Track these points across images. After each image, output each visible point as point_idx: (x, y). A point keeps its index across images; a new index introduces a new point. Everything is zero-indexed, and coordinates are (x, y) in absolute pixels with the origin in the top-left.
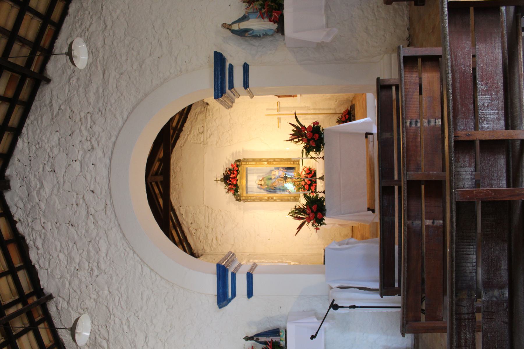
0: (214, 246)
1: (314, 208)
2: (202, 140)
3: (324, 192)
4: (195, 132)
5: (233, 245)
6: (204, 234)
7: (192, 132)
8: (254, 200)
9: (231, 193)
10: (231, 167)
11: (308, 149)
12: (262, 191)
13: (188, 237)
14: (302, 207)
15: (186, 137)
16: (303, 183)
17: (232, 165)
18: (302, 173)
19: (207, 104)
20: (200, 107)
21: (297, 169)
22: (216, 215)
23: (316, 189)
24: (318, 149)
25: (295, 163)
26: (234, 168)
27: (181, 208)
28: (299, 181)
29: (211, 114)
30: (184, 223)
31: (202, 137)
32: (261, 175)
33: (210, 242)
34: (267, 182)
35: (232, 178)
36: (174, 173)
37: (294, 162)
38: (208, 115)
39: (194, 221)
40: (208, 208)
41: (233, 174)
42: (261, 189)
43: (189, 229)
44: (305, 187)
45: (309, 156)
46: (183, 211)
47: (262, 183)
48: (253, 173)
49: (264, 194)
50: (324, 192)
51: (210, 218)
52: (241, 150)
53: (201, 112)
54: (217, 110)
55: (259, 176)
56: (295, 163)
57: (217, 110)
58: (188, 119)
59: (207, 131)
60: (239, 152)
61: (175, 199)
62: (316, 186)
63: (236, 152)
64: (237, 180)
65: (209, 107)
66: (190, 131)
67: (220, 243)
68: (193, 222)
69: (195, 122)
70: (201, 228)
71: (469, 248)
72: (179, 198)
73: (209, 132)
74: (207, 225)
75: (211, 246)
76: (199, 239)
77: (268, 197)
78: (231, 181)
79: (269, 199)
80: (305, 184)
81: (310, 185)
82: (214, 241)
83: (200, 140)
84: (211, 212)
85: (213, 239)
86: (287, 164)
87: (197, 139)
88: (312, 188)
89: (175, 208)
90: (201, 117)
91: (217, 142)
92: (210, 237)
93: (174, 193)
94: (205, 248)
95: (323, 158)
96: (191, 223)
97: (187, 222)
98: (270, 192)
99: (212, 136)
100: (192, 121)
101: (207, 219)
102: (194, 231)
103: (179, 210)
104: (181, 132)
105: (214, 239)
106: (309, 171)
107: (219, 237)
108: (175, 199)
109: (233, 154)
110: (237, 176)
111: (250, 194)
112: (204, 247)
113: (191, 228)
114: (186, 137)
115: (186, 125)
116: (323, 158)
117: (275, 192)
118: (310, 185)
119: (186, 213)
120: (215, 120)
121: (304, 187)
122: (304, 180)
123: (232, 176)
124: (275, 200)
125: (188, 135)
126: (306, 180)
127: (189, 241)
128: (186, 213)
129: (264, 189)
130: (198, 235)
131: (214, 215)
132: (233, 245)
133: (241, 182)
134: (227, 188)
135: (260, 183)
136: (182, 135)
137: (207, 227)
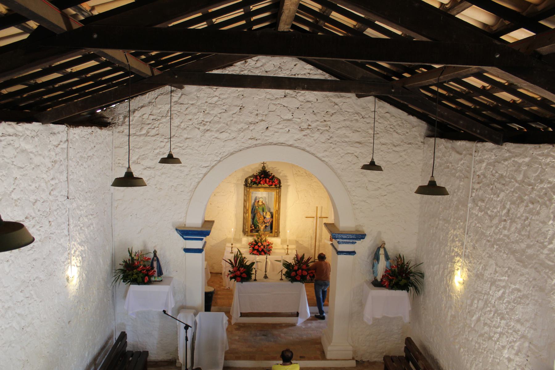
16: (260, 244)
34: (261, 208)
47: (260, 203)
60: (287, 182)
79: (245, 207)
81: (258, 250)
109: (286, 176)
117: (252, 213)
126: (262, 247)
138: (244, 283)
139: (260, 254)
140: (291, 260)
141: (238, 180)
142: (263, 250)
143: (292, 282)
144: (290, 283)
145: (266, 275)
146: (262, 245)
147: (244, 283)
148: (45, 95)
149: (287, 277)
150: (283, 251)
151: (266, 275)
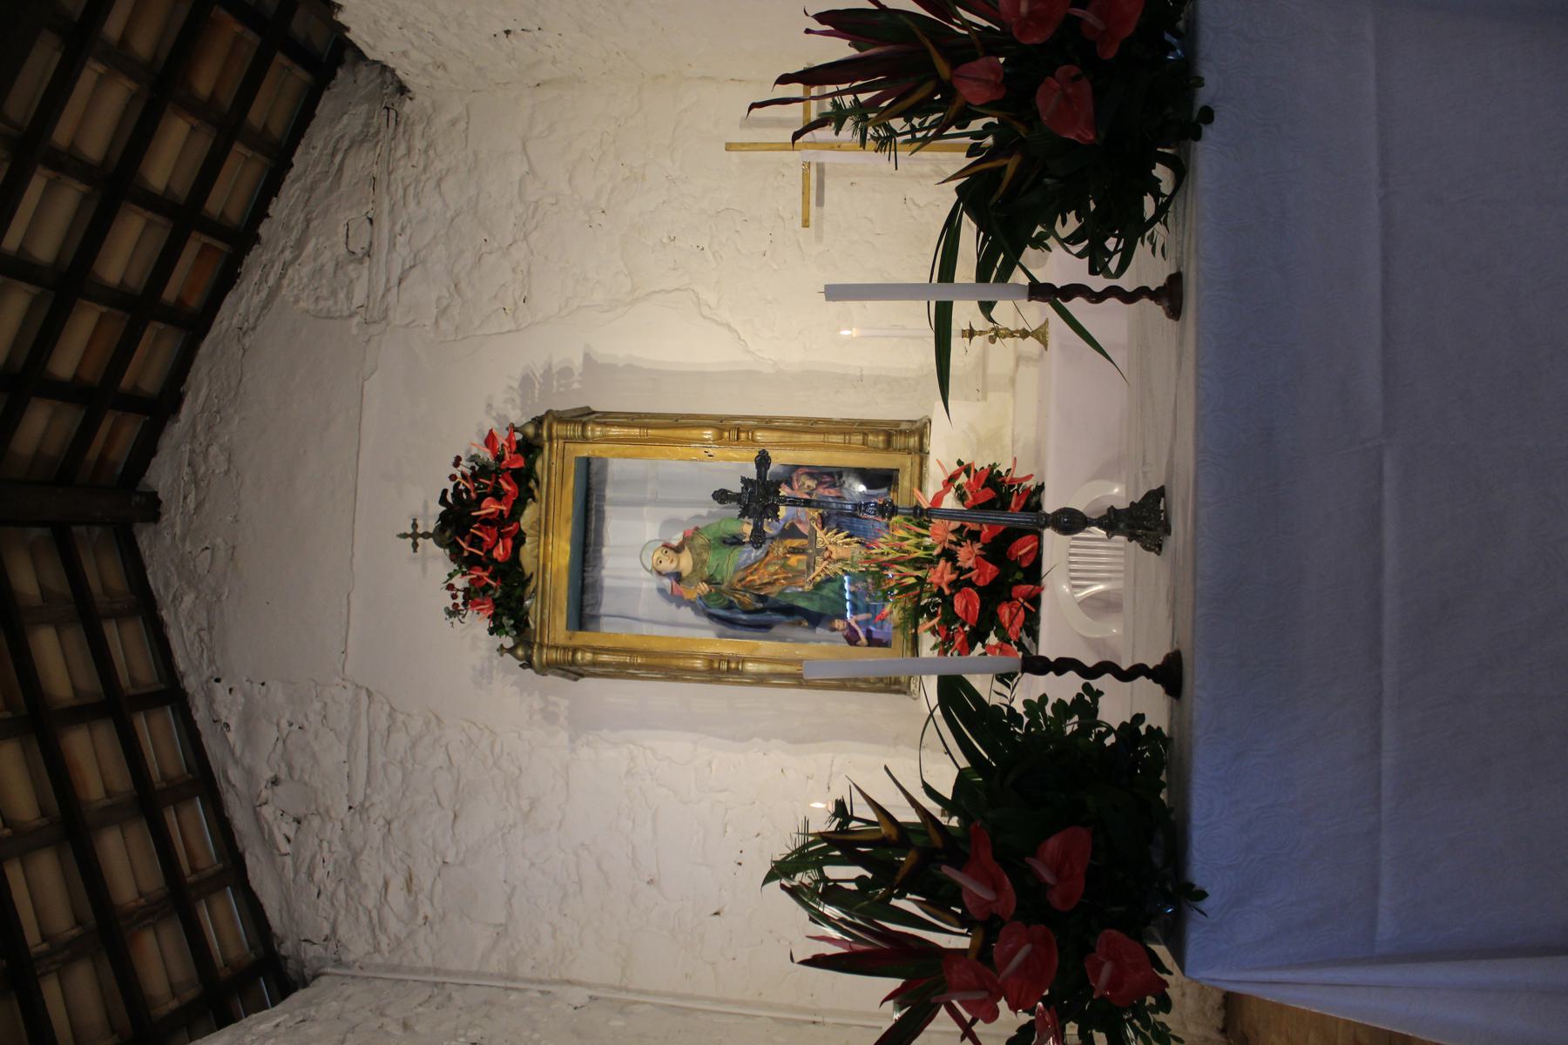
0: (393, 925)
1: (1059, 860)
2: (359, 297)
3: (1169, 675)
4: (326, 246)
5: (502, 932)
6: (338, 847)
7: (309, 249)
8: (620, 671)
9: (477, 623)
10: (487, 455)
11: (1001, 212)
12: (687, 614)
13: (250, 861)
14: (907, 815)
15: (272, 280)
16: (941, 574)
17: (490, 440)
18: (938, 498)
19: (402, 89)
20: (365, 107)
21: (905, 482)
22: (414, 745)
23: (1031, 626)
24: (1113, 223)
25: (899, 441)
26: (499, 458)
27: (220, 690)
28: (917, 563)
29: (419, 144)
30: (234, 774)
31: (361, 279)
32: (685, 513)
33: (370, 900)
34: (712, 559)
35: (486, 521)
36: (196, 483)
37: (889, 436)
38: (402, 150)
39: (290, 768)
40: (369, 694)
41: (498, 495)
42: (679, 601)
43: (257, 817)
44: (959, 604)
45: (1018, 277)
46: (229, 708)
47: (686, 562)
48: (640, 503)
49: (706, 639)
50: (1169, 675)
51: (379, 759)
52: (578, 362)
53: (365, 138)
54: (454, 123)
55: (670, 523)
56: (899, 441)
57: (454, 123)
58: (292, 174)
59: (393, 245)
60: (566, 372)
61: (189, 635)
62: (1035, 601)
63: (548, 372)
64: (519, 539)
65: (408, 107)
66: (300, 245)
67: (425, 909)
68: (283, 776)
69: (331, 190)
70: (325, 815)
71: (584, 439)
72: (210, 628)
73: (402, 251)
74: (358, 799)
75: (377, 926)
76: (310, 875)
77: (710, 659)
78: (476, 542)
79: (719, 672)
80: (956, 585)
81: (994, 594)
82: (397, 896)
83: (349, 298)
84: (383, 723)
85: (386, 885)
86: (846, 447)
87: (334, 293)
88: (1005, 612)
89: (191, 683)
90: (360, 163)
91: (443, 312)
92: (370, 873)
93: (188, 600)
94: (343, 932)
95: (1170, 295)
96: (275, 782)
97: (250, 774)
98: (730, 622)
99: (415, 273)
100: (312, 189)
101: (362, 763)
102: (289, 828)
103: (211, 702)
104: (247, 251)
105: (397, 883)
106: (990, 494)
107: (425, 878)
108: (189, 635)
109: (527, 381)
110: (516, 513)
111: (611, 631)
112: (334, 931)
113: (267, 811)
114: (272, 280)
115: (279, 208)
116: (1170, 295)
117: (763, 627)
118: (994, 594)
119: (248, 718)
120: (438, 185)
121: (948, 602)
122: (948, 555)
123: (490, 507)
124: (760, 680)
125: (285, 267)
126: (967, 555)
127: (254, 885)
128: (248, 718)
129: (691, 603)
130: (307, 855)
131: (400, 740)
132: (502, 932)
133: (550, 554)
134: (460, 582)
135: (668, 566)
136: (255, 259)
137: (358, 810)
138: (1199, 872)
139: (1034, 573)
140: (906, 194)
141: (550, 717)
142: (997, 550)
143: (1192, 125)
144: (1207, 154)
145: (1112, 521)
146: (948, 555)
147: (1206, 862)
148: (1027, 959)
149: (1134, 229)
150: (1029, 374)
151: (1112, 521)
